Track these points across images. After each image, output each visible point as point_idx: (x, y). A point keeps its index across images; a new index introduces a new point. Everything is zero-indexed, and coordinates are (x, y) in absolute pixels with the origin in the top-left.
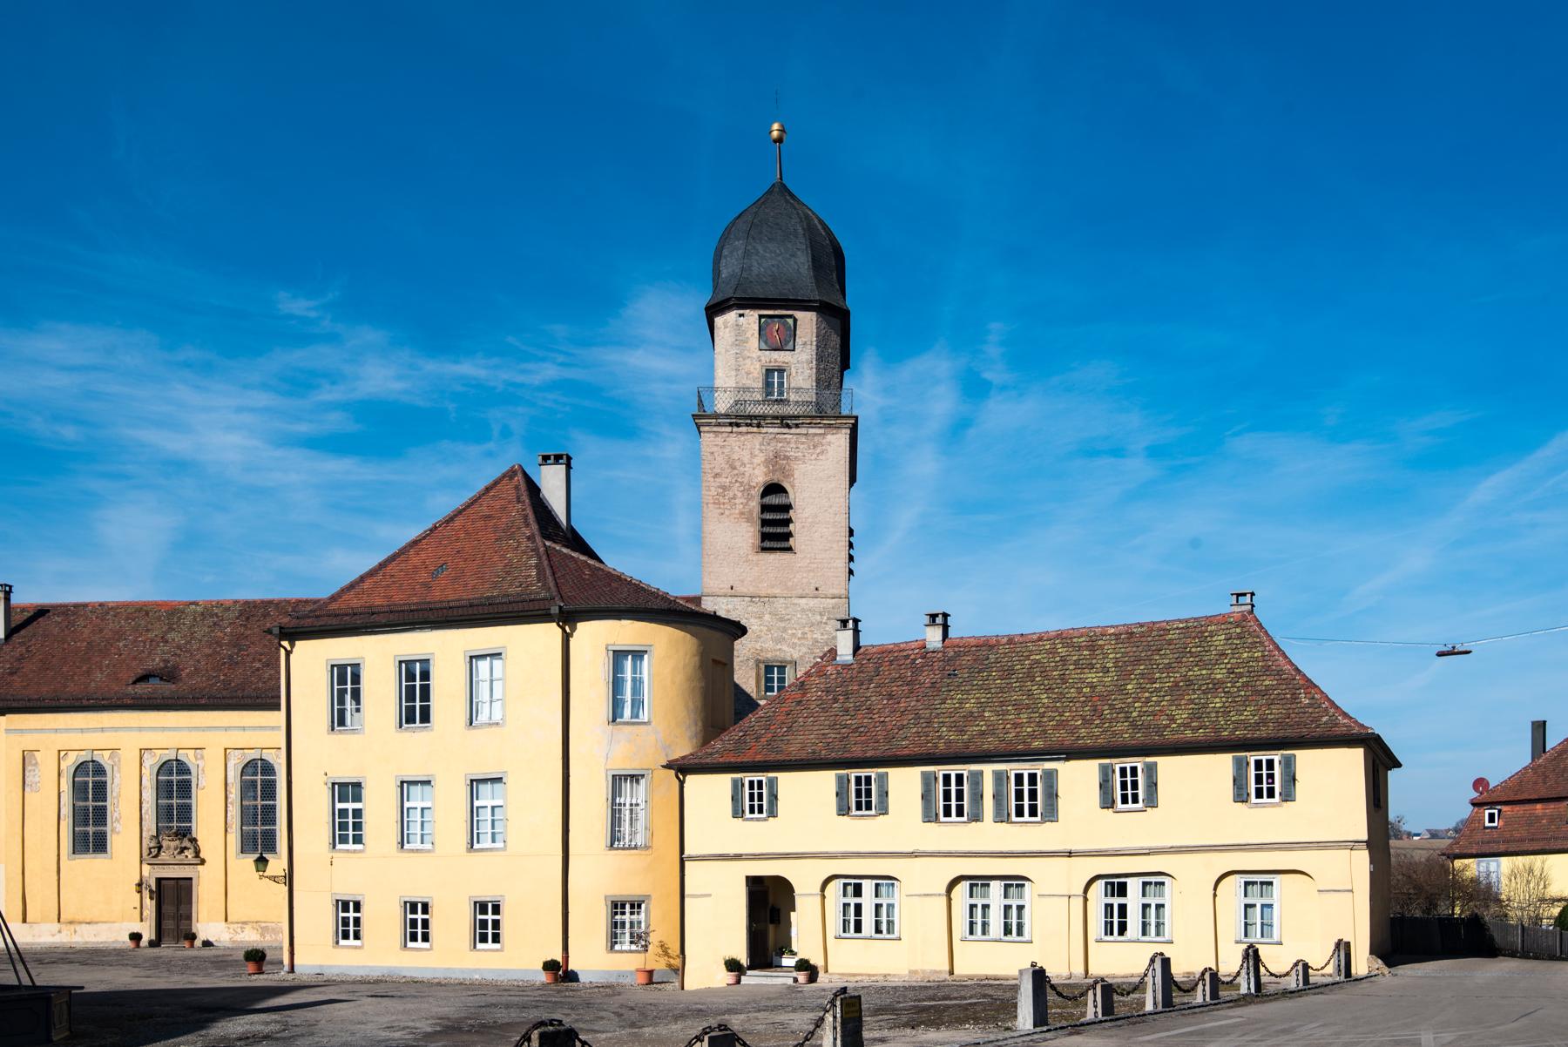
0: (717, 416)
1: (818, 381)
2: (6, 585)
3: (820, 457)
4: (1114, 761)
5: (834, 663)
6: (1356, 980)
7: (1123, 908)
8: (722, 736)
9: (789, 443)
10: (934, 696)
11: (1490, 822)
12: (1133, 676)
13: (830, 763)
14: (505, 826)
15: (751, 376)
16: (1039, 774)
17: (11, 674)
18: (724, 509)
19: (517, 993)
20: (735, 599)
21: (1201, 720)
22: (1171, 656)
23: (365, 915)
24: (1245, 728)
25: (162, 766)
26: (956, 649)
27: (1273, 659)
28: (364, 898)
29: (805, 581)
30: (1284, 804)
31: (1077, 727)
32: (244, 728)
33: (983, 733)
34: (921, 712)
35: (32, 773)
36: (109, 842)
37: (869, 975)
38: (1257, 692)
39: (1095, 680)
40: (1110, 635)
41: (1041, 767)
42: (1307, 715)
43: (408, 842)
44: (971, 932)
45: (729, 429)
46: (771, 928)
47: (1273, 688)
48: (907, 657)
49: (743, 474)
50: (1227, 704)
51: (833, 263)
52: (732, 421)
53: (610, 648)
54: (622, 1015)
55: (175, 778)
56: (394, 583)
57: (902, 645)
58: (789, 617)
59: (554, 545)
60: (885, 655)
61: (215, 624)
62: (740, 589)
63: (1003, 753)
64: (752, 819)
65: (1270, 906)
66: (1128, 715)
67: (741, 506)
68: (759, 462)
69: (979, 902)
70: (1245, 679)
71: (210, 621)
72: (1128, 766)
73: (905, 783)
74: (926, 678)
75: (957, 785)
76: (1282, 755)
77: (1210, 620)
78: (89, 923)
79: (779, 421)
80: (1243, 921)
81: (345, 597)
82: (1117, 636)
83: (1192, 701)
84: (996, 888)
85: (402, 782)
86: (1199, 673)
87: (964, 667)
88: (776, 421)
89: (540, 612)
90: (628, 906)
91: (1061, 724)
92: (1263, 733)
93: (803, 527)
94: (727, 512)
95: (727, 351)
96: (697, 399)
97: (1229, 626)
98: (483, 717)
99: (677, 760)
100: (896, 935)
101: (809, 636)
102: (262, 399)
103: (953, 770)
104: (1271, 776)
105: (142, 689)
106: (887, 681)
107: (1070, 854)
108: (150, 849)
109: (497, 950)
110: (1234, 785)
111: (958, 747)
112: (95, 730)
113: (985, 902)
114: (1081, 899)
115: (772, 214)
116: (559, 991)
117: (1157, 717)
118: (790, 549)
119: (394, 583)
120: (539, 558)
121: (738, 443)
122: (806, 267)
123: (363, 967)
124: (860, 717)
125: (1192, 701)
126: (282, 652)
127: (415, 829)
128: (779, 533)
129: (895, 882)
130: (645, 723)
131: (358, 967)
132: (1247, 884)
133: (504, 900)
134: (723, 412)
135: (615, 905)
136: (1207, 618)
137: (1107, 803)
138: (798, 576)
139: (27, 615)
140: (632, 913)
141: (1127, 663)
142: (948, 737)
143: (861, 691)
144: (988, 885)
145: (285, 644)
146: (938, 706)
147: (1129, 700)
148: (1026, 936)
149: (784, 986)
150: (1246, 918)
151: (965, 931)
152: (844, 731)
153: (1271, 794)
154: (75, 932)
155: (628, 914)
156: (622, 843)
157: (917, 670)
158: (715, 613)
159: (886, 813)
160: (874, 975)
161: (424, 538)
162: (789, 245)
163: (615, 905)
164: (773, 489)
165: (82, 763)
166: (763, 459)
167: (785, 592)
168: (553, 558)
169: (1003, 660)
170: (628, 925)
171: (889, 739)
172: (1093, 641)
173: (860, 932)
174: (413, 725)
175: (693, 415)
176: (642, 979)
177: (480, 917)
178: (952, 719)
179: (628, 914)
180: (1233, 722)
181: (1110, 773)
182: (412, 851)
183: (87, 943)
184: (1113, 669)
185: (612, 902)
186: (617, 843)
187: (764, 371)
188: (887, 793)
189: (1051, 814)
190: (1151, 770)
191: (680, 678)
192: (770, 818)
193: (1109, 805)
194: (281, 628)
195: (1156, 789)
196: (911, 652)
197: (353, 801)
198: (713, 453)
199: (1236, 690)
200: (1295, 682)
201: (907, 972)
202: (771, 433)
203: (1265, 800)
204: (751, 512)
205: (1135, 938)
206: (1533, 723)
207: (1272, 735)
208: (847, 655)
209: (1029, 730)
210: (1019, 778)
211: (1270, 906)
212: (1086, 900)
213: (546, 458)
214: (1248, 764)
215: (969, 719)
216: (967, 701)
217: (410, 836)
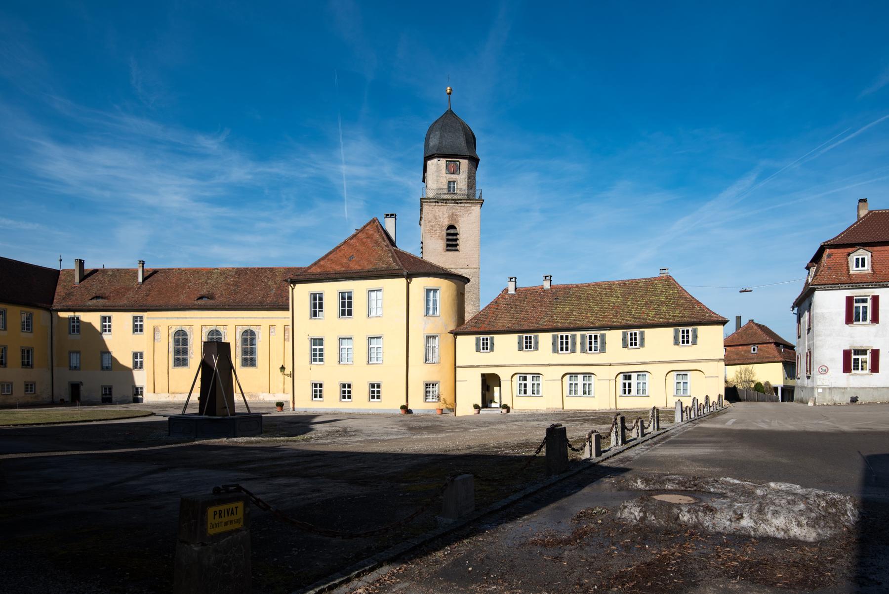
0: (430, 199)
1: (468, 186)
7: (630, 385)
9: (457, 209)
17: (147, 296)
25: (210, 332)
30: (693, 346)
32: (243, 318)
33: (574, 320)
37: (530, 410)
45: (434, 204)
46: (487, 392)
48: (537, 292)
61: (226, 277)
64: (484, 352)
69: (574, 383)
71: (224, 276)
72: (633, 332)
73: (545, 339)
77: (655, 279)
78: (181, 393)
81: (314, 267)
82: (619, 284)
83: (654, 309)
84: (580, 377)
90: (431, 385)
92: (685, 320)
94: (433, 236)
95: (433, 174)
98: (373, 314)
102: (192, 182)
103: (564, 334)
104: (688, 336)
105: (200, 302)
107: (610, 365)
111: (566, 326)
112: (183, 318)
118: (457, 250)
120: (392, 253)
125: (654, 309)
126: (290, 288)
127: (345, 356)
129: (540, 375)
137: (625, 346)
140: (433, 388)
142: (560, 322)
145: (292, 285)
147: (630, 308)
153: (688, 342)
154: (175, 397)
159: (538, 350)
160: (532, 410)
161: (342, 245)
162: (457, 134)
163: (427, 385)
164: (451, 227)
165: (177, 331)
170: (347, 397)
171: (537, 322)
172: (610, 287)
173: (539, 394)
177: (371, 389)
182: (344, 364)
189: (603, 349)
190: (642, 334)
197: (319, 345)
198: (428, 213)
203: (685, 344)
204: (443, 236)
206: (736, 317)
211: (687, 383)
213: (387, 215)
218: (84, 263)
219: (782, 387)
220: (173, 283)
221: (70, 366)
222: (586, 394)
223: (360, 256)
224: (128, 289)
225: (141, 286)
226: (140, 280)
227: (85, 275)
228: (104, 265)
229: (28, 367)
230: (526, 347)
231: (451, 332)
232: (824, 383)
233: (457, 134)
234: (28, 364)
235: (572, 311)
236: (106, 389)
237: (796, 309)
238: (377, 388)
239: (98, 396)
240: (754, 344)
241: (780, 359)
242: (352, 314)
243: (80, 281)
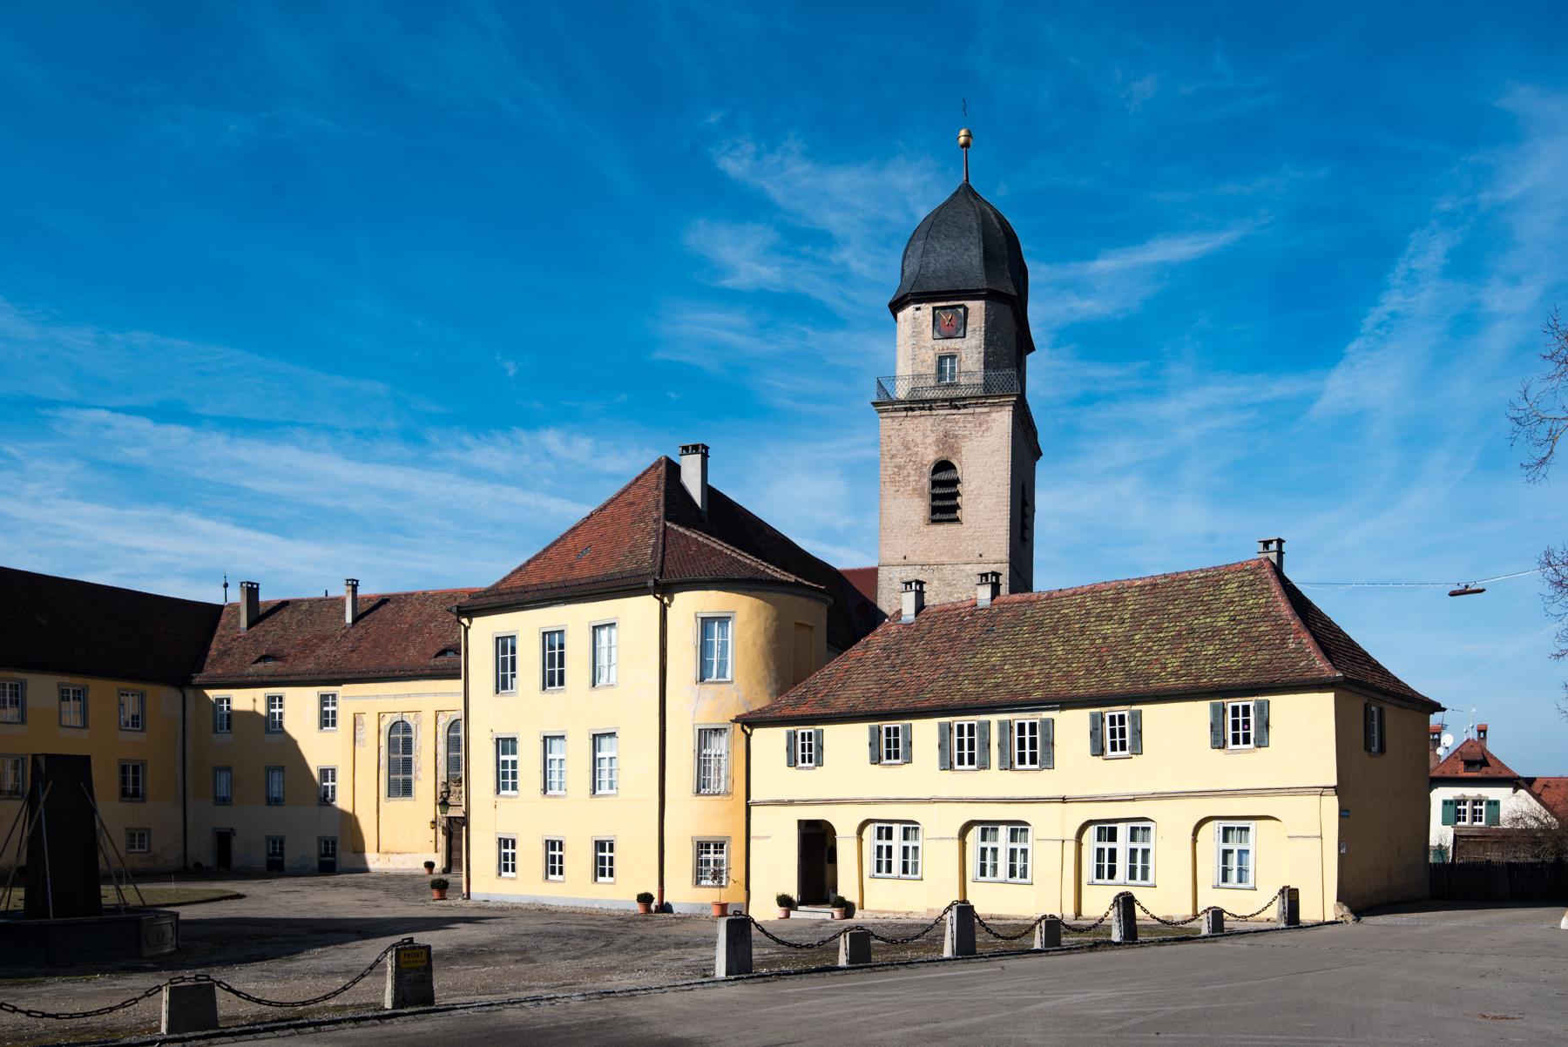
2: (353, 580)
3: (985, 434)
4: (1103, 710)
6: (1302, 927)
7: (1113, 852)
12: (1143, 627)
13: (862, 716)
15: (925, 364)
17: (352, 651)
18: (899, 486)
20: (908, 568)
25: (452, 724)
27: (1275, 605)
31: (1078, 678)
33: (997, 685)
35: (360, 732)
36: (413, 787)
37: (894, 912)
38: (1251, 639)
41: (1039, 717)
43: (550, 789)
45: (904, 414)
47: (1266, 633)
49: (917, 454)
51: (1006, 253)
53: (699, 615)
56: (550, 565)
58: (955, 582)
59: (675, 527)
62: (912, 558)
63: (1005, 704)
66: (1127, 664)
67: (914, 483)
68: (931, 441)
70: (1243, 626)
73: (925, 733)
75: (969, 735)
78: (398, 853)
84: (1004, 832)
85: (545, 738)
86: (1203, 621)
90: (712, 847)
91: (1067, 675)
93: (969, 499)
94: (902, 490)
97: (1244, 574)
98: (603, 681)
100: (1028, 880)
103: (966, 720)
104: (1247, 722)
108: (442, 793)
109: (611, 883)
115: (951, 213)
118: (957, 520)
119: (550, 565)
121: (912, 426)
123: (517, 895)
125: (1187, 650)
130: (728, 682)
136: (1227, 566)
139: (371, 604)
140: (715, 853)
145: (465, 621)
155: (712, 853)
157: (962, 625)
160: (899, 913)
161: (581, 525)
162: (964, 241)
164: (943, 466)
165: (454, 722)
166: (934, 439)
170: (712, 863)
172: (1118, 594)
174: (553, 688)
178: (977, 672)
179: (712, 853)
183: (397, 869)
187: (937, 358)
188: (911, 743)
189: (1049, 762)
191: (761, 640)
193: (1098, 753)
194: (458, 607)
198: (890, 436)
201: (925, 911)
202: (942, 415)
203: (1241, 746)
204: (922, 488)
205: (1003, 879)
208: (909, 615)
209: (1037, 681)
211: (1247, 852)
213: (685, 448)
218: (258, 588)
220: (405, 623)
221: (215, 797)
224: (324, 639)
225: (348, 632)
226: (349, 619)
227: (259, 613)
228: (326, 592)
229: (135, 799)
234: (136, 794)
236: (274, 843)
239: (260, 858)
243: (249, 627)
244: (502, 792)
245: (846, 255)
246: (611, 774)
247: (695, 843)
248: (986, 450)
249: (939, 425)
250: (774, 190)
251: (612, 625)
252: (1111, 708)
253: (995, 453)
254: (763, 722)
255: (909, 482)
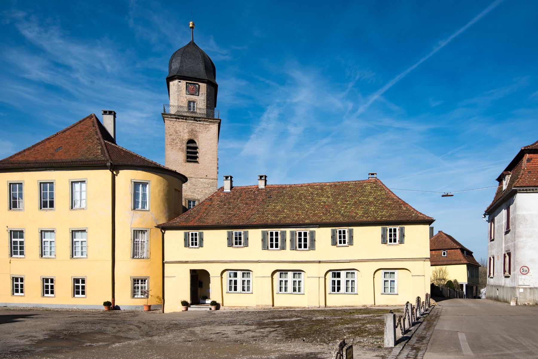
0: (171, 115)
3: (208, 132)
4: (337, 228)
5: (223, 192)
7: (339, 282)
8: (179, 216)
9: (197, 126)
10: (264, 204)
11: (444, 255)
12: (339, 199)
14: (87, 249)
16: (308, 232)
18: (173, 147)
19: (92, 316)
21: (368, 214)
22: (352, 193)
23: (25, 283)
24: (386, 217)
26: (270, 189)
28: (25, 277)
29: (202, 173)
33: (285, 217)
34: (259, 210)
37: (240, 307)
39: (325, 200)
40: (328, 185)
41: (309, 230)
42: (406, 213)
43: (44, 255)
44: (280, 291)
45: (175, 120)
46: (199, 289)
48: (252, 191)
49: (180, 135)
50: (376, 209)
51: (212, 69)
52: (176, 117)
53: (133, 181)
54: (140, 327)
55: (136, 282)
57: (249, 187)
59: (108, 142)
60: (243, 190)
63: (294, 224)
65: (394, 281)
67: (180, 146)
69: (284, 279)
72: (342, 230)
74: (260, 198)
76: (400, 227)
77: (364, 181)
79: (193, 119)
80: (384, 286)
81: (16, 157)
82: (331, 186)
83: (363, 208)
84: (290, 274)
85: (42, 231)
87: (274, 195)
88: (192, 119)
89: (102, 165)
90: (140, 281)
91: (314, 215)
92: (392, 219)
93: (202, 155)
95: (174, 94)
96: (163, 108)
97: (371, 184)
98: (77, 206)
99: (161, 225)
100: (251, 292)
101: (204, 191)
103: (274, 230)
104: (395, 235)
106: (244, 199)
107: (320, 262)
109: (84, 297)
110: (382, 237)
113: (286, 279)
114: (324, 278)
115: (190, 50)
116: (110, 314)
117: (351, 213)
118: (197, 162)
119: (39, 153)
120: (102, 146)
121: (178, 125)
122: (203, 69)
124: (235, 211)
125: (363, 208)
127: (47, 250)
128: (193, 156)
130: (147, 211)
131: (23, 304)
132: (385, 273)
133: (87, 278)
134: (173, 114)
135: (134, 280)
136: (362, 181)
137: (334, 243)
138: (200, 171)
140: (142, 283)
141: (336, 195)
142: (271, 219)
143: (235, 202)
144: (287, 273)
146: (266, 208)
148: (302, 292)
149: (207, 312)
150: (384, 285)
151: (278, 290)
152: (229, 215)
153: (395, 241)
156: (138, 256)
157: (256, 195)
158: (176, 171)
160: (242, 307)
161: (53, 137)
162: (197, 61)
163: (134, 280)
164: (191, 141)
166: (187, 131)
167: (195, 176)
168: (109, 147)
169: (289, 193)
170: (140, 288)
172: (322, 187)
175: (162, 114)
176: (146, 309)
178: (272, 212)
180: (380, 215)
181: (335, 232)
184: (331, 197)
185: (133, 279)
186: (135, 256)
187: (188, 101)
188: (248, 239)
189: (313, 247)
190: (351, 232)
191: (162, 194)
192: (200, 248)
195: (353, 238)
196: (253, 189)
199: (378, 204)
200: (399, 202)
201: (255, 306)
207: (396, 220)
209: (302, 216)
210: (300, 234)
211: (394, 281)
212: (325, 279)
214: (387, 230)
215: (279, 212)
216: (277, 206)
217: (46, 252)
219: (466, 285)
222: (296, 291)
223: (68, 147)
230: (236, 244)
231: (158, 227)
232: (525, 283)
233: (197, 61)
235: (283, 208)
237: (487, 216)
238: (82, 283)
240: (444, 250)
241: (466, 262)
242: (54, 206)
244: (14, 256)
245: (78, 75)
246: (82, 249)
247: (132, 280)
248: (208, 138)
249: (189, 126)
250: (46, 45)
251: (83, 182)
252: (340, 228)
253: (212, 140)
254: (173, 228)
255: (177, 145)
